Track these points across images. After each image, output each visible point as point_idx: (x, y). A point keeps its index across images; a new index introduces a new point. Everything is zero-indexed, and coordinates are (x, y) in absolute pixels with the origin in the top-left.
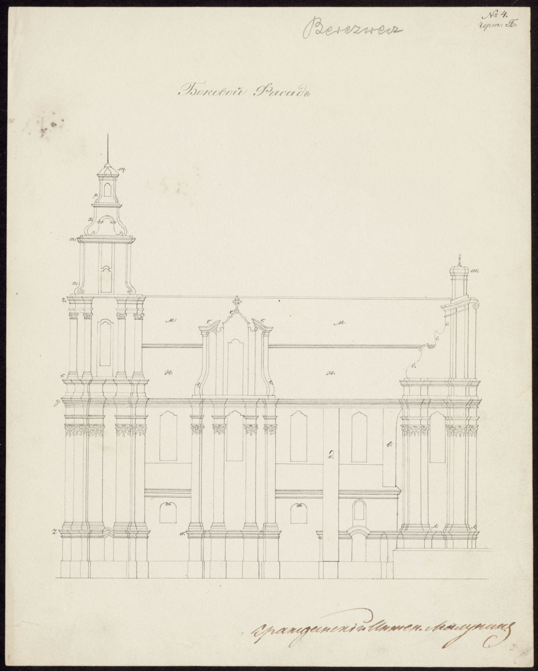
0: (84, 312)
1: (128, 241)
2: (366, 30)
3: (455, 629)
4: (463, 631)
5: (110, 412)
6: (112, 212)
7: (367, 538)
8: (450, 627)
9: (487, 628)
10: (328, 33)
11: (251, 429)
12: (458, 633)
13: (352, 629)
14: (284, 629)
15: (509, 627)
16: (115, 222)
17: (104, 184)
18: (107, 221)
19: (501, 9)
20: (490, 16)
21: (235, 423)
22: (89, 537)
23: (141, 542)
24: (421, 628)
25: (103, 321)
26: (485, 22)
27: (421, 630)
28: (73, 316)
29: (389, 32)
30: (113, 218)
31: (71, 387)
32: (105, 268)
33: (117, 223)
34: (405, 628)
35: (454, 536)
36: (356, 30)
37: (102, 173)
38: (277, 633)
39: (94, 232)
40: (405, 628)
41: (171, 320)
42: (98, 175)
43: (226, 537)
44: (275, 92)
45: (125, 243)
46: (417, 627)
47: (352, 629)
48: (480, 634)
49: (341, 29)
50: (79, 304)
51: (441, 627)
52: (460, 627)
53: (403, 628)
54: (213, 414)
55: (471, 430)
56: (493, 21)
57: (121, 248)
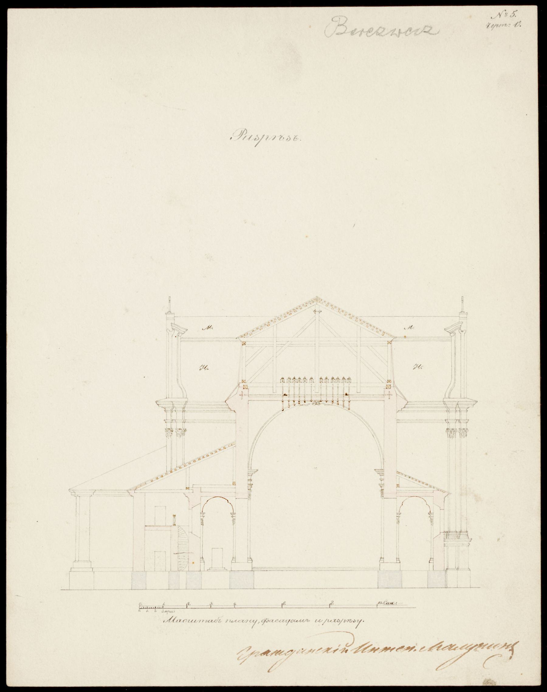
3: (442, 649)
4: (464, 651)
10: (369, 34)
12: (459, 652)
13: (335, 651)
14: (328, 649)
19: (510, 9)
26: (492, 22)
27: (415, 650)
29: (418, 33)
41: (209, 327)
44: (248, 137)
46: (409, 649)
47: (335, 651)
48: (484, 652)
51: (439, 646)
52: (460, 647)
53: (395, 649)
55: (464, 432)
56: (503, 20)
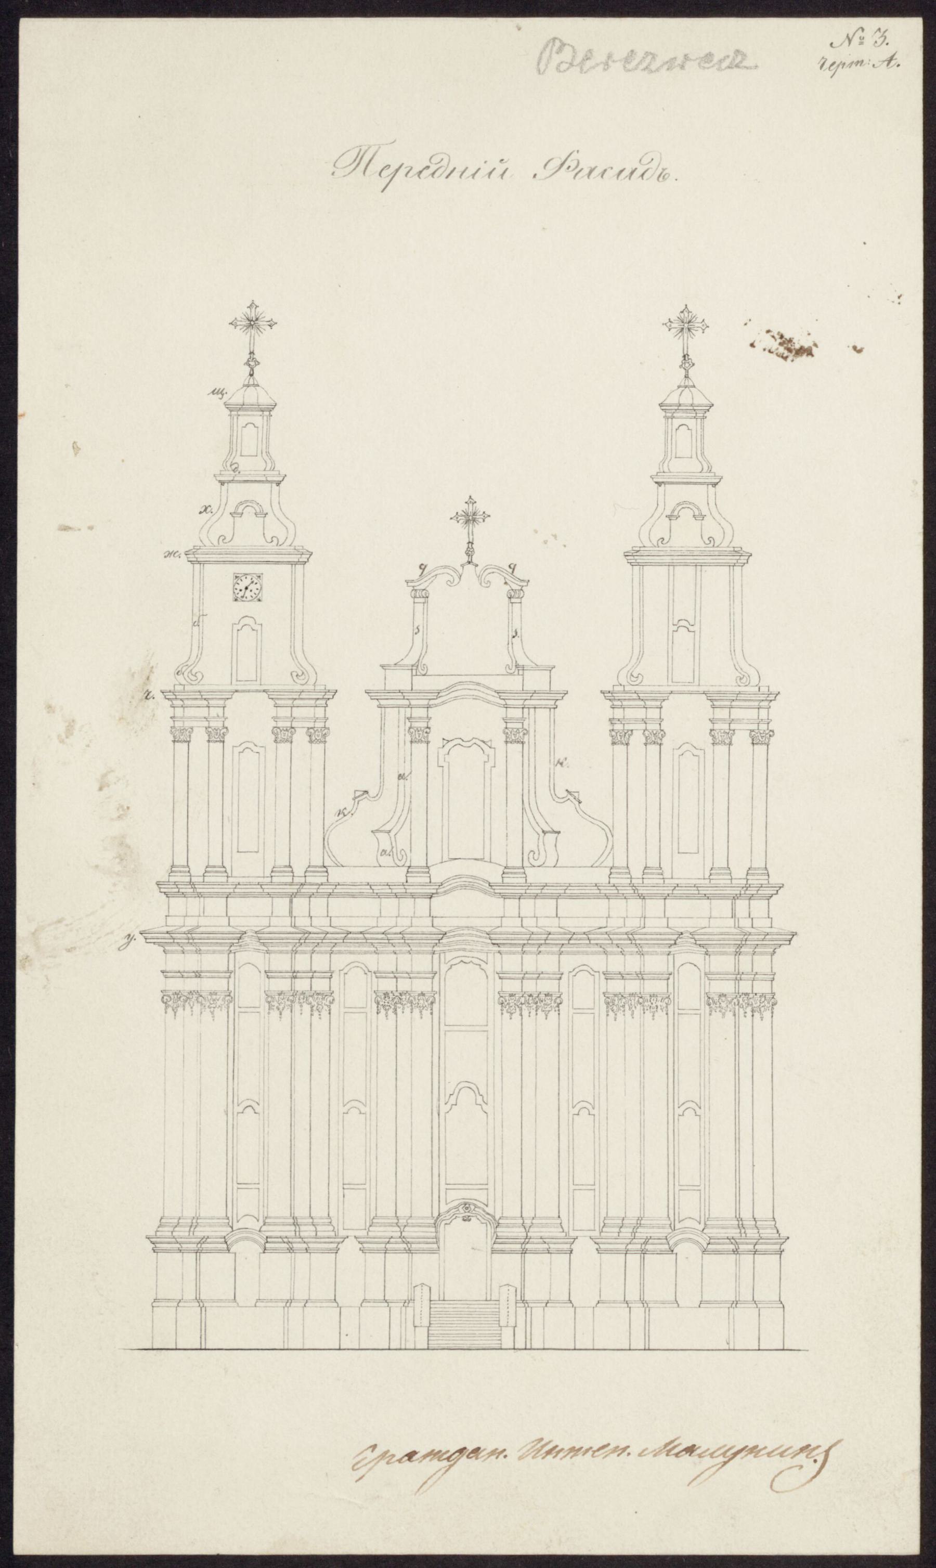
0: (206, 724)
1: (294, 558)
2: (670, 64)
5: (250, 958)
6: (697, 494)
7: (704, 1251)
8: (690, 1450)
9: (769, 1454)
11: (389, 1002)
14: (414, 1453)
15: (827, 1452)
16: (703, 517)
17: (676, 426)
18: (686, 515)
20: (847, 41)
21: (468, 991)
22: (524, 1252)
23: (767, 1263)
24: (628, 1450)
25: (244, 746)
28: (620, 738)
30: (698, 509)
31: (178, 904)
32: (682, 623)
33: (708, 519)
34: (594, 1452)
35: (184, 1246)
36: (648, 63)
37: (674, 399)
38: (400, 1461)
39: (222, 538)
40: (594, 1452)
42: (661, 405)
43: (755, 1252)
45: (289, 563)
49: (615, 57)
50: (744, 713)
53: (590, 1453)
54: (163, 969)
57: (716, 578)
